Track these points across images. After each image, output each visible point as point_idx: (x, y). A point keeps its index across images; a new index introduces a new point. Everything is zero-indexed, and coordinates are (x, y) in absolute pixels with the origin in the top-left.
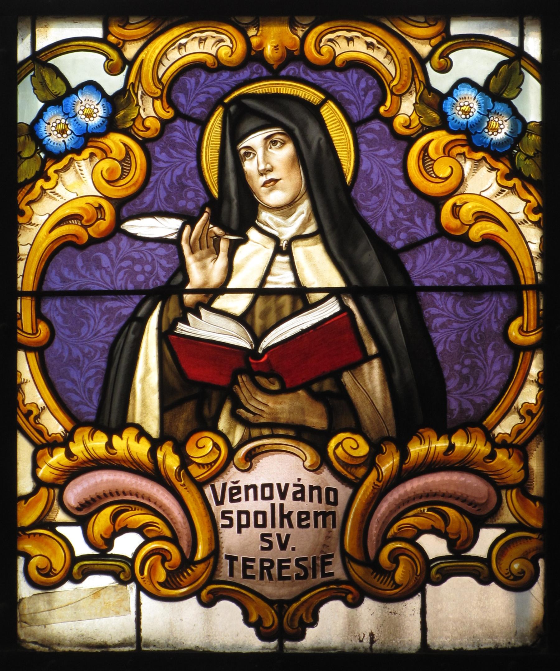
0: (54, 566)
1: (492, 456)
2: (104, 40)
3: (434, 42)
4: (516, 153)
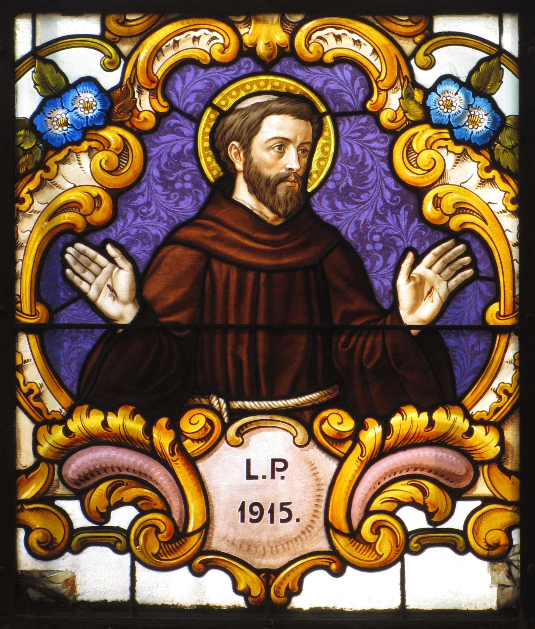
0: (55, 536)
1: (470, 433)
2: (102, 37)
3: (418, 39)
4: (496, 145)
